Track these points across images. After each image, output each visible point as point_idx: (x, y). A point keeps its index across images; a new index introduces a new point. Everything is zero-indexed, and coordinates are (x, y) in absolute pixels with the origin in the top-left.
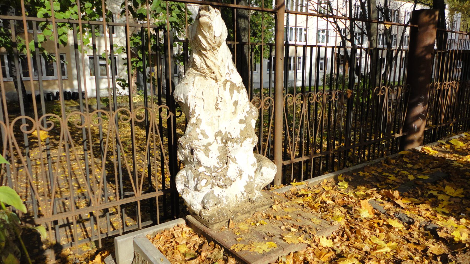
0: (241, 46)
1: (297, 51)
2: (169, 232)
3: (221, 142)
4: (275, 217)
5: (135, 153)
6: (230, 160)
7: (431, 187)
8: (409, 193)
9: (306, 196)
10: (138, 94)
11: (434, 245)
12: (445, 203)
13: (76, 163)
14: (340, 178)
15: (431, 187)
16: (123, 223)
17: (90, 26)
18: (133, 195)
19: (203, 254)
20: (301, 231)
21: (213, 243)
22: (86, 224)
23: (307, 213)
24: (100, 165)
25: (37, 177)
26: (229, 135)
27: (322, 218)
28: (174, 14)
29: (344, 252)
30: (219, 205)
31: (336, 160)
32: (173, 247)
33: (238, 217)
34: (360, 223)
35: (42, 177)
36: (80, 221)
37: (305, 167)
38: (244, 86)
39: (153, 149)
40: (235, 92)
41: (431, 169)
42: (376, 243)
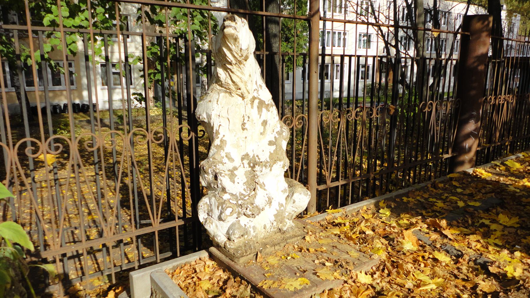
0: (271, 57)
1: (333, 61)
2: (190, 266)
3: (248, 166)
4: (308, 250)
5: (152, 174)
6: (258, 186)
7: (482, 215)
8: (458, 222)
9: (343, 225)
10: (156, 106)
11: (484, 281)
12: (498, 234)
13: (86, 186)
14: (381, 204)
15: (482, 215)
16: (139, 254)
17: (101, 35)
18: (150, 225)
19: (228, 291)
20: (337, 266)
21: (238, 279)
22: (98, 255)
23: (344, 245)
24: (113, 188)
25: (42, 202)
26: (257, 158)
27: (360, 251)
28: (196, 21)
29: (385, 289)
30: (246, 236)
31: (377, 183)
32: (195, 283)
33: (267, 250)
34: (402, 257)
35: (49, 202)
36: (91, 252)
37: (343, 191)
38: (273, 103)
39: (173, 169)
40: (264, 110)
41: (483, 194)
42: (420, 278)
